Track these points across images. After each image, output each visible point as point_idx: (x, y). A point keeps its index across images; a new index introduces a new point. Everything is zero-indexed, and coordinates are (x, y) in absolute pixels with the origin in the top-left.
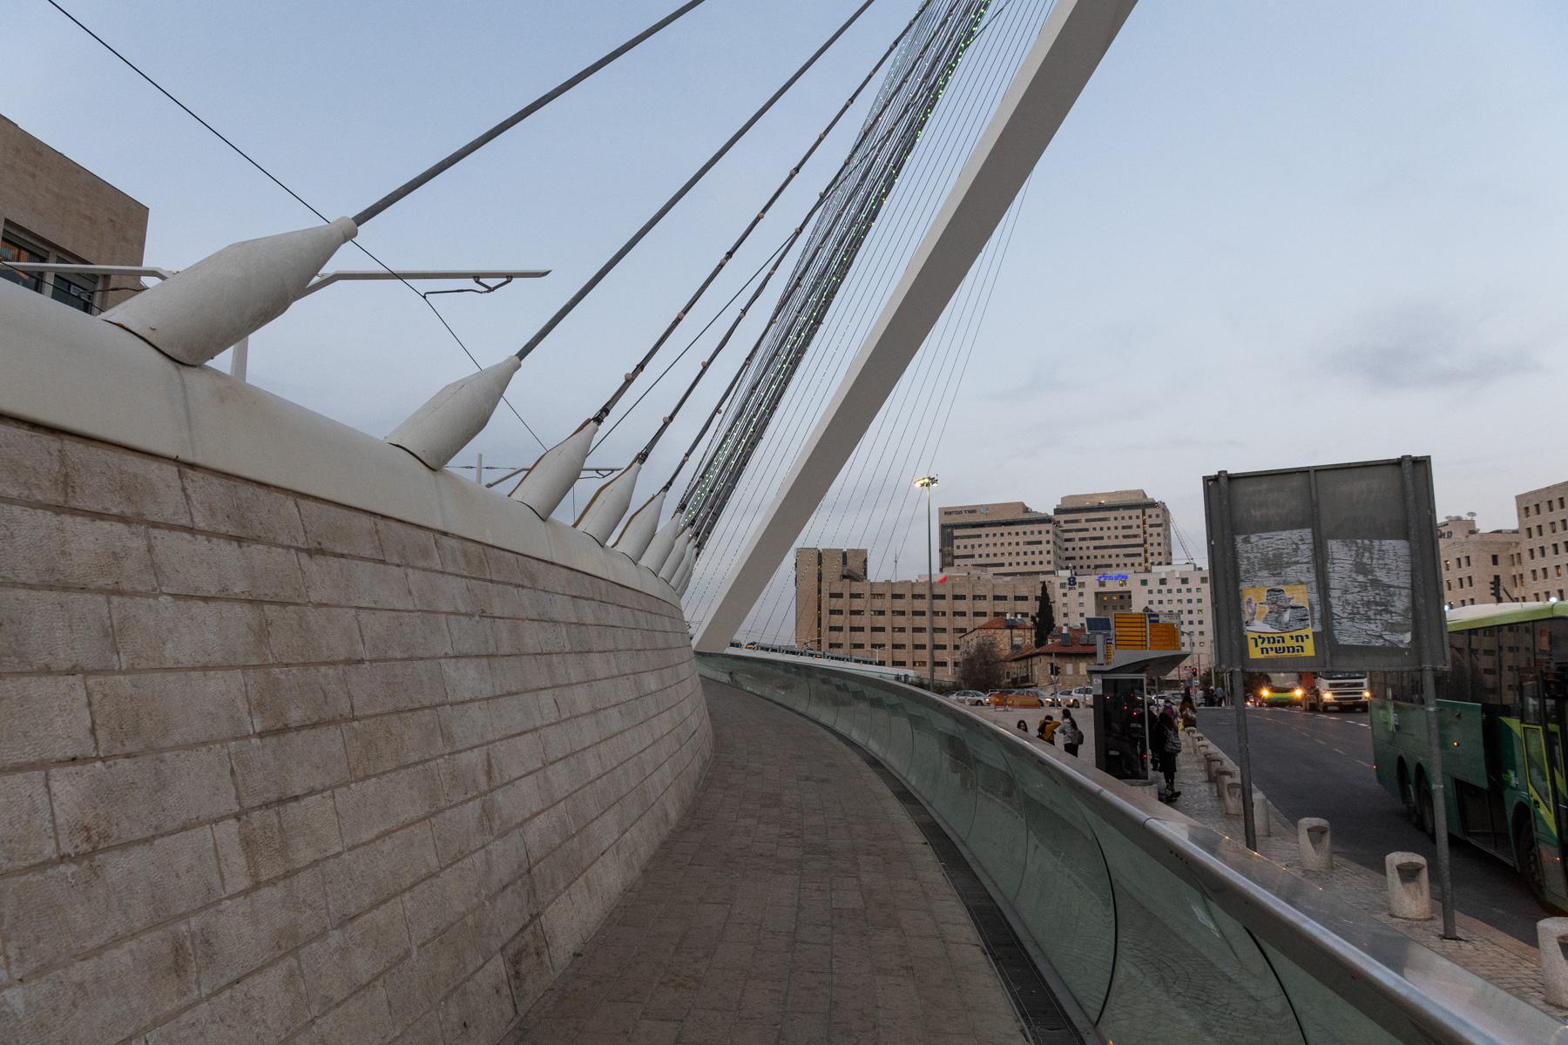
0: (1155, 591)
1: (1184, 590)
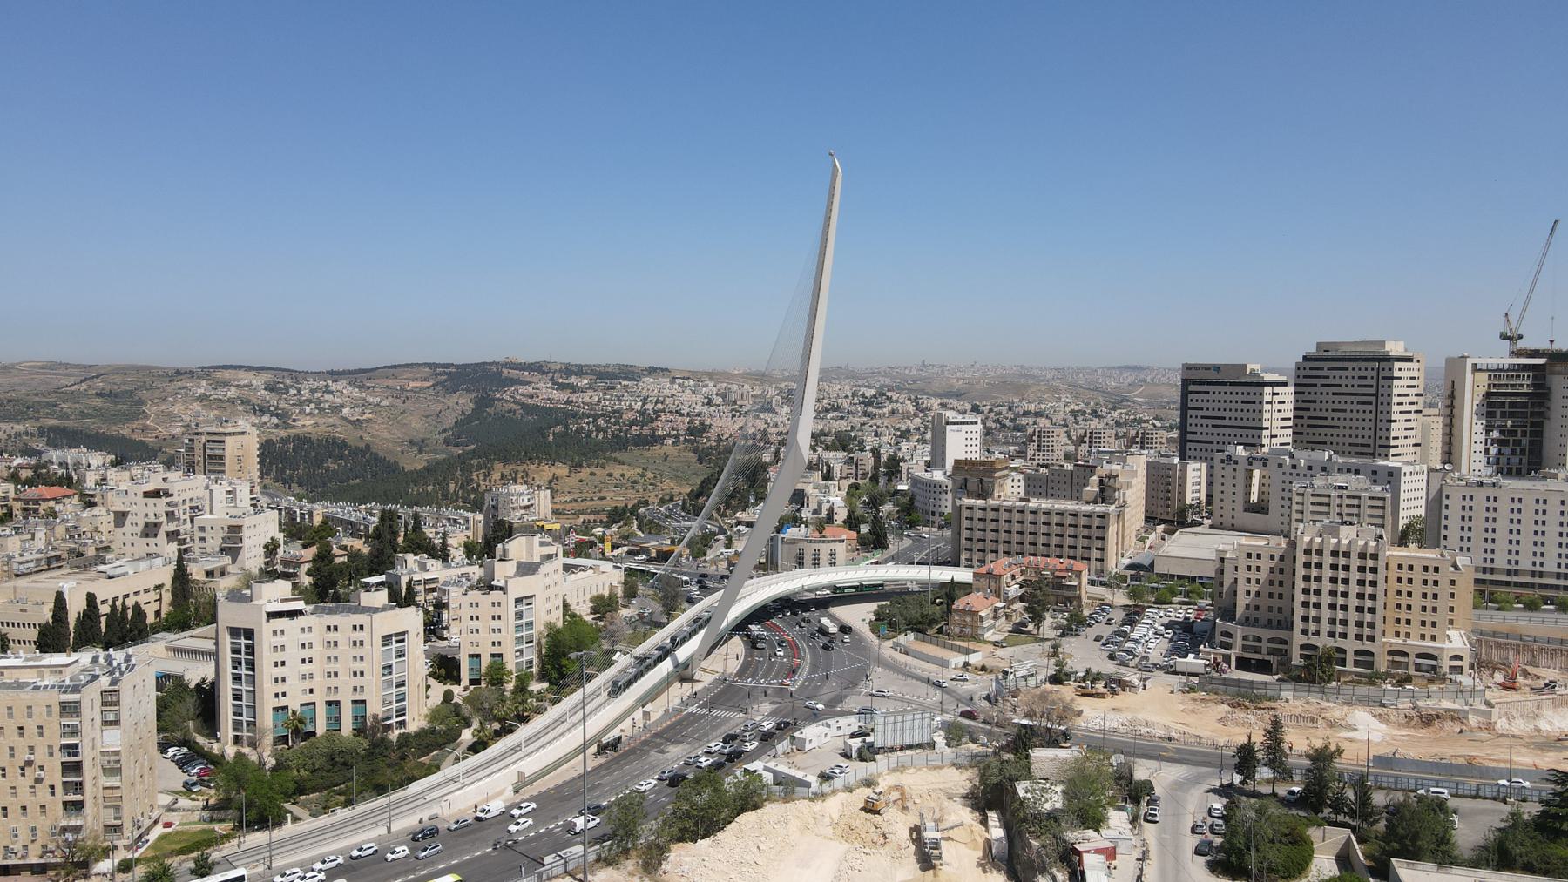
0: (1288, 474)
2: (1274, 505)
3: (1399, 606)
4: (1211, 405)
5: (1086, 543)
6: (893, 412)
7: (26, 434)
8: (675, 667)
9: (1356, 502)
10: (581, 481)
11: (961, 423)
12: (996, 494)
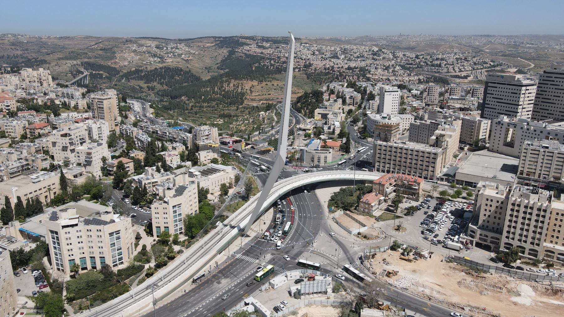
0: (525, 132)
1: (534, 134)
2: (517, 144)
3: (554, 230)
4: (497, 93)
5: (427, 164)
6: (384, 58)
7: (77, 65)
8: (239, 231)
9: (551, 154)
10: (262, 87)
11: (391, 92)
12: (392, 140)
